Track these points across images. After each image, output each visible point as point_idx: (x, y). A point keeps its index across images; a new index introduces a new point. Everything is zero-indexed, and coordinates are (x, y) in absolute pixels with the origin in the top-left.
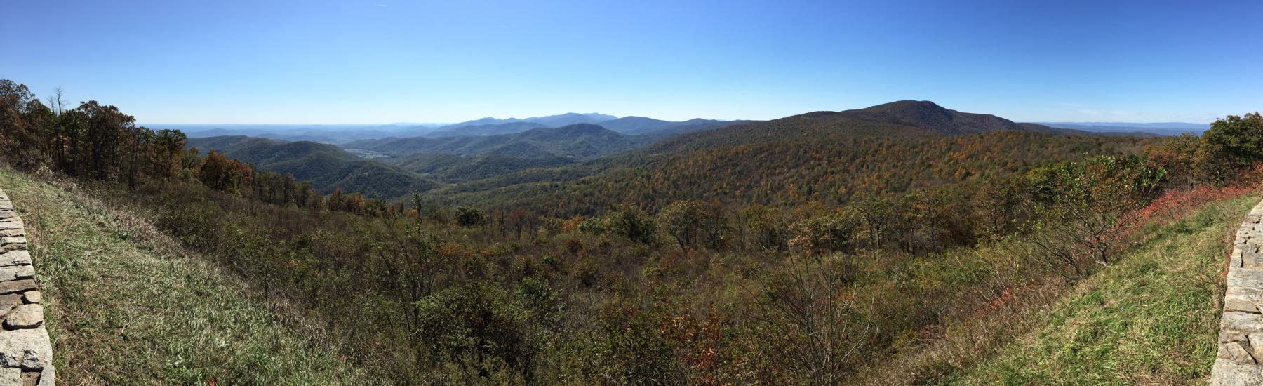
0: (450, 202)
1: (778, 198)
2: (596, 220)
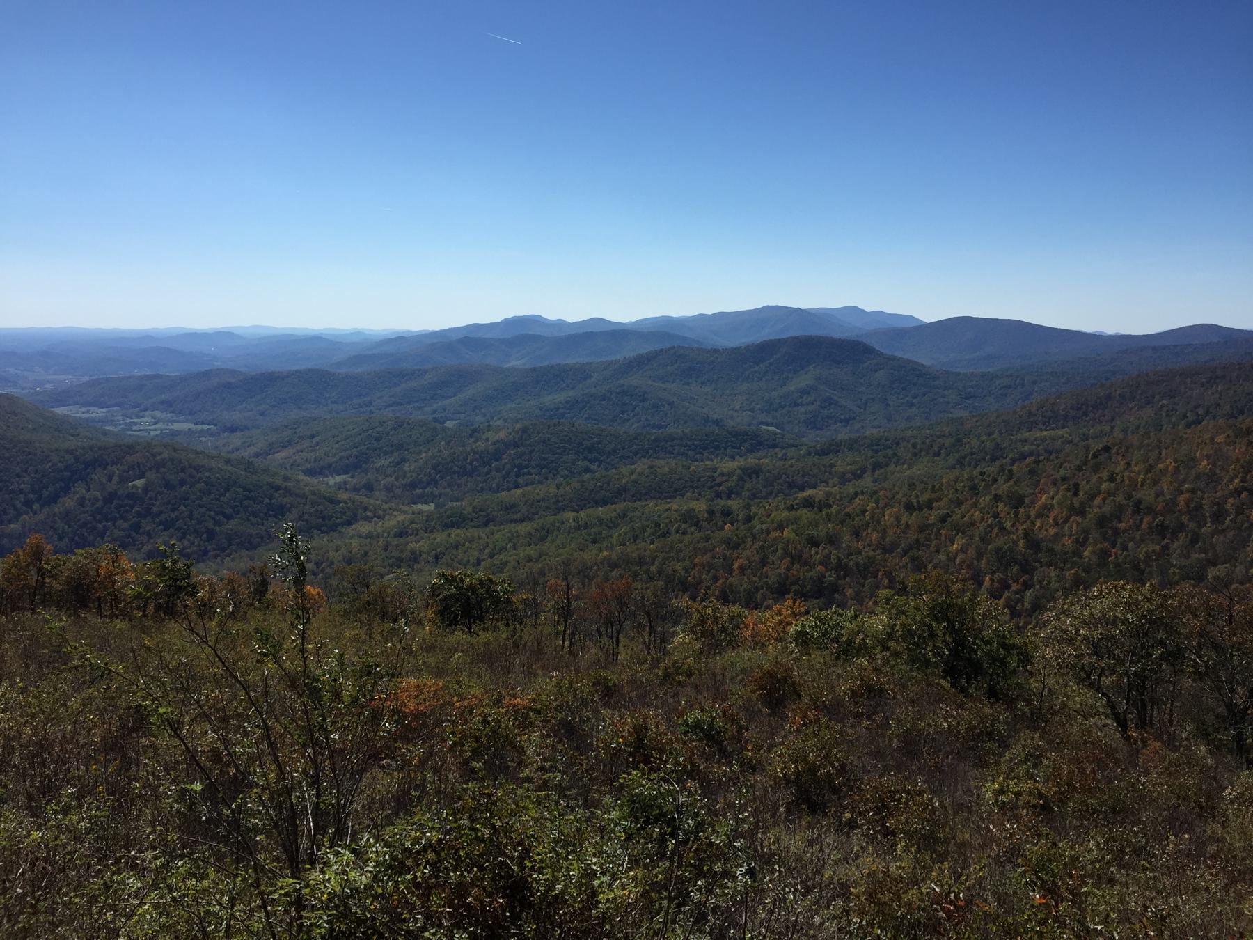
0: (415, 557)
2: (844, 620)
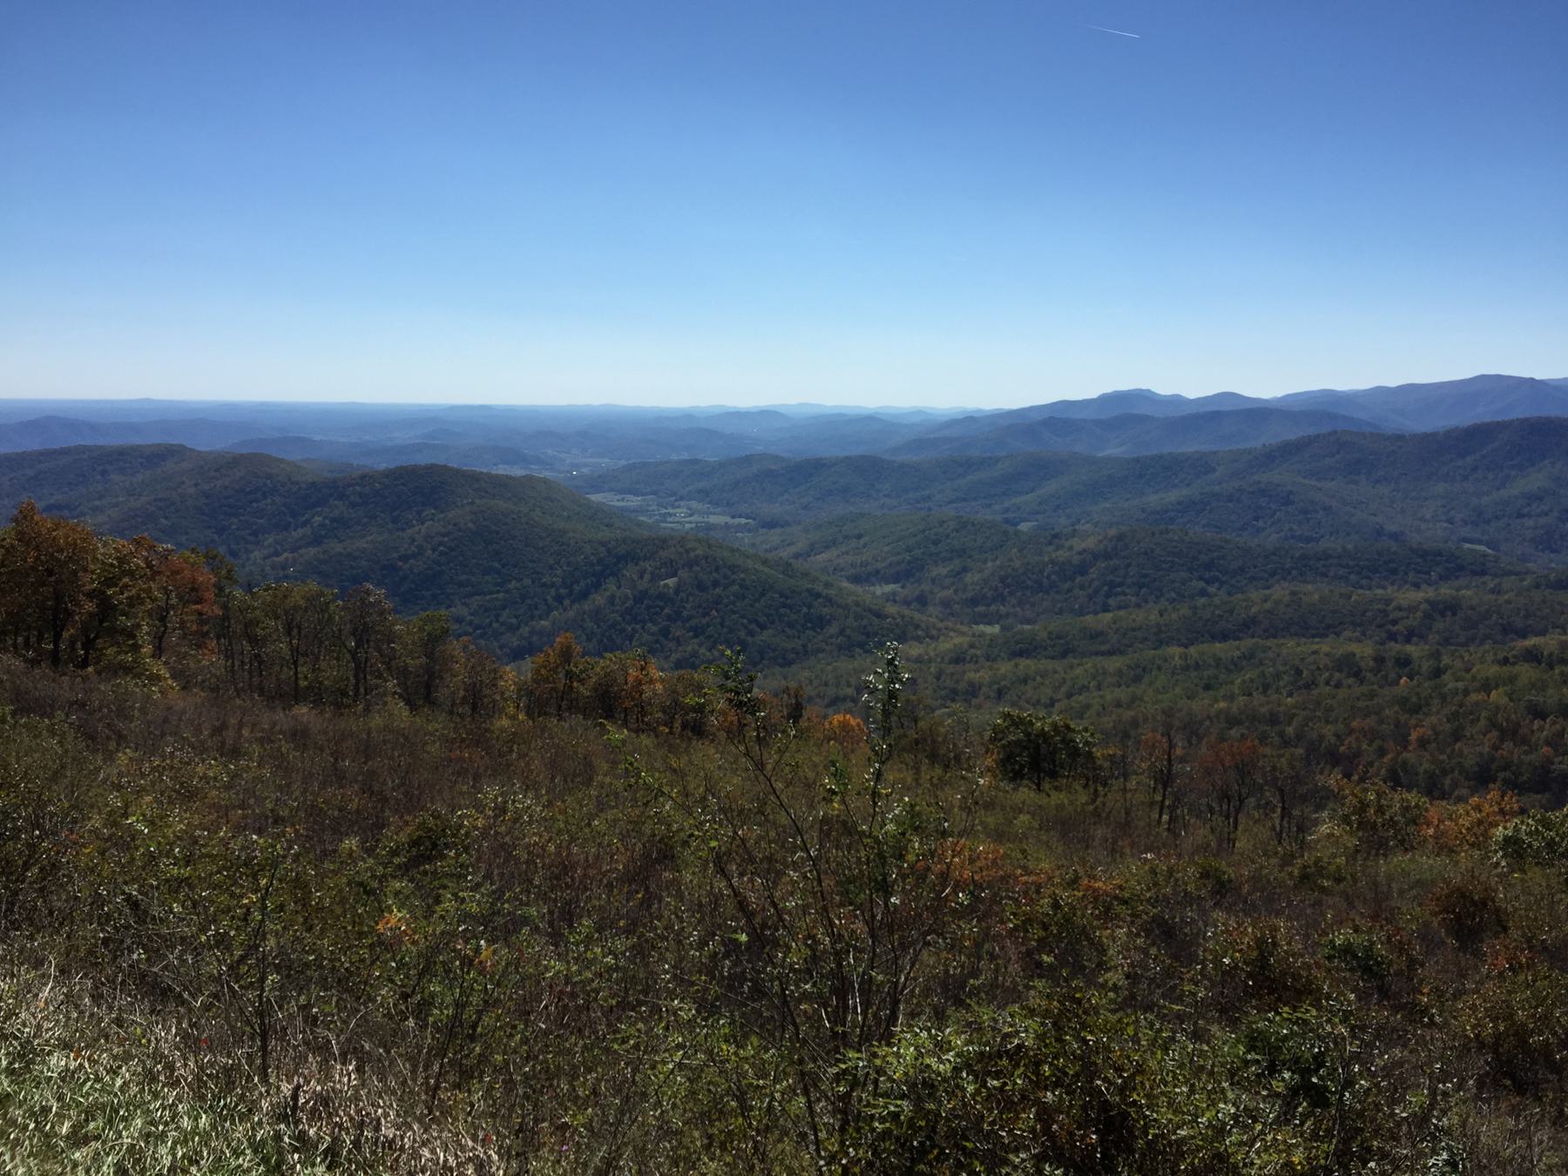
0: (973, 691)
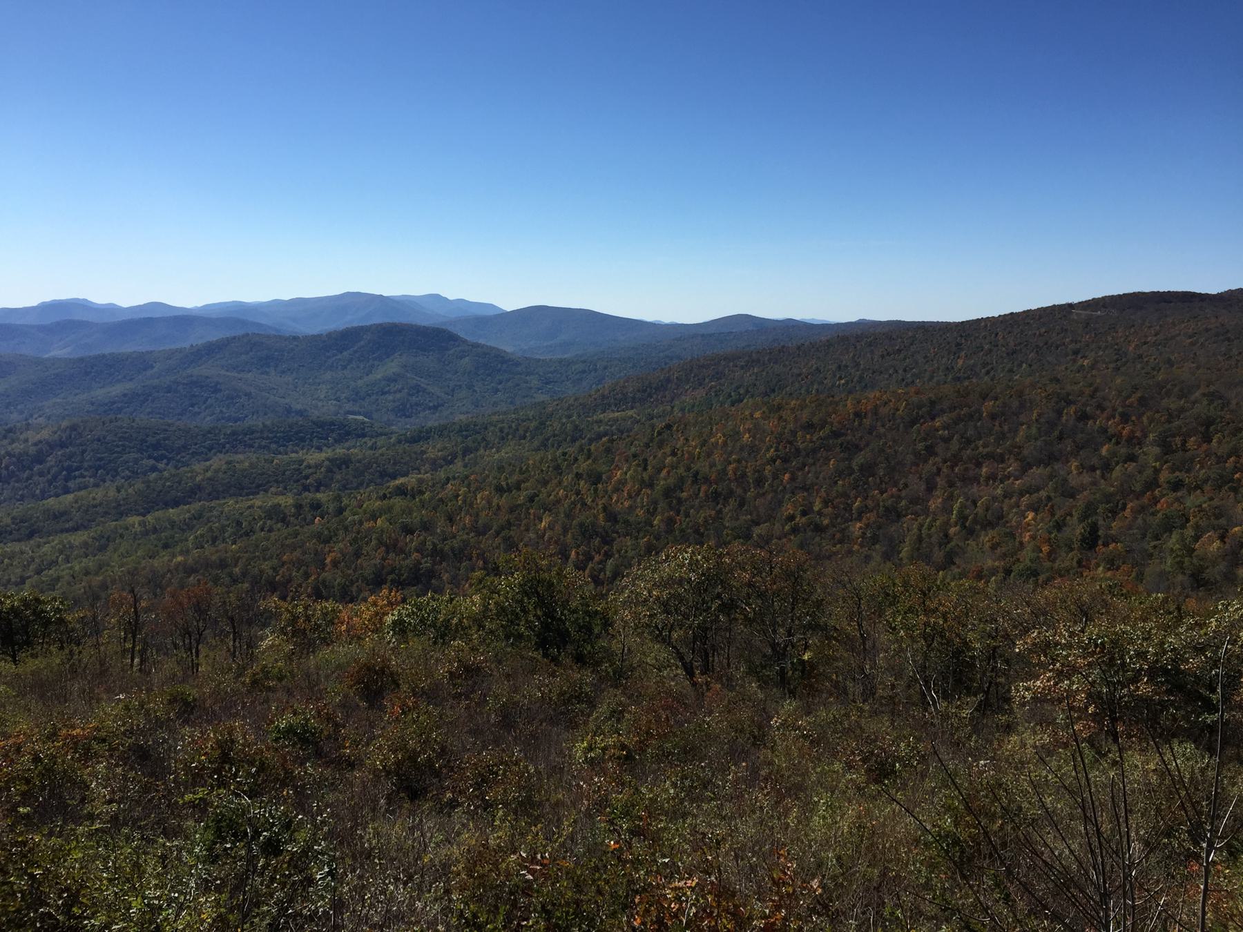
1: (981, 552)
2: (438, 604)
